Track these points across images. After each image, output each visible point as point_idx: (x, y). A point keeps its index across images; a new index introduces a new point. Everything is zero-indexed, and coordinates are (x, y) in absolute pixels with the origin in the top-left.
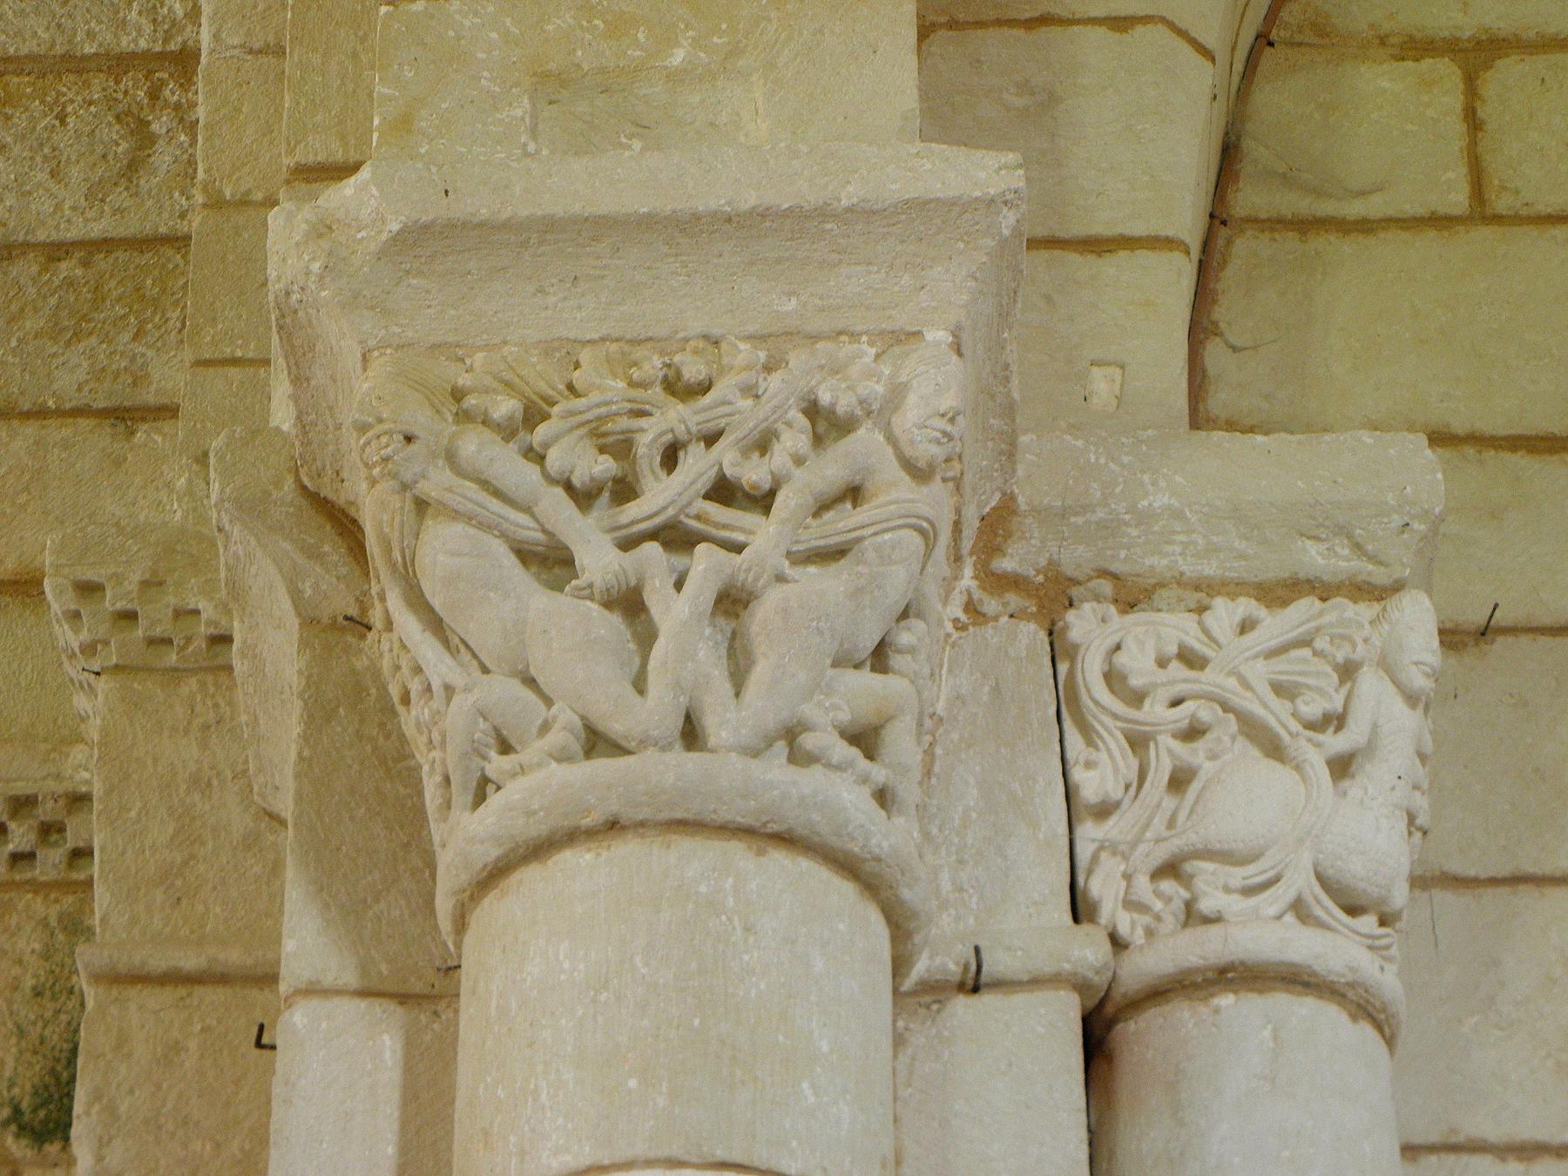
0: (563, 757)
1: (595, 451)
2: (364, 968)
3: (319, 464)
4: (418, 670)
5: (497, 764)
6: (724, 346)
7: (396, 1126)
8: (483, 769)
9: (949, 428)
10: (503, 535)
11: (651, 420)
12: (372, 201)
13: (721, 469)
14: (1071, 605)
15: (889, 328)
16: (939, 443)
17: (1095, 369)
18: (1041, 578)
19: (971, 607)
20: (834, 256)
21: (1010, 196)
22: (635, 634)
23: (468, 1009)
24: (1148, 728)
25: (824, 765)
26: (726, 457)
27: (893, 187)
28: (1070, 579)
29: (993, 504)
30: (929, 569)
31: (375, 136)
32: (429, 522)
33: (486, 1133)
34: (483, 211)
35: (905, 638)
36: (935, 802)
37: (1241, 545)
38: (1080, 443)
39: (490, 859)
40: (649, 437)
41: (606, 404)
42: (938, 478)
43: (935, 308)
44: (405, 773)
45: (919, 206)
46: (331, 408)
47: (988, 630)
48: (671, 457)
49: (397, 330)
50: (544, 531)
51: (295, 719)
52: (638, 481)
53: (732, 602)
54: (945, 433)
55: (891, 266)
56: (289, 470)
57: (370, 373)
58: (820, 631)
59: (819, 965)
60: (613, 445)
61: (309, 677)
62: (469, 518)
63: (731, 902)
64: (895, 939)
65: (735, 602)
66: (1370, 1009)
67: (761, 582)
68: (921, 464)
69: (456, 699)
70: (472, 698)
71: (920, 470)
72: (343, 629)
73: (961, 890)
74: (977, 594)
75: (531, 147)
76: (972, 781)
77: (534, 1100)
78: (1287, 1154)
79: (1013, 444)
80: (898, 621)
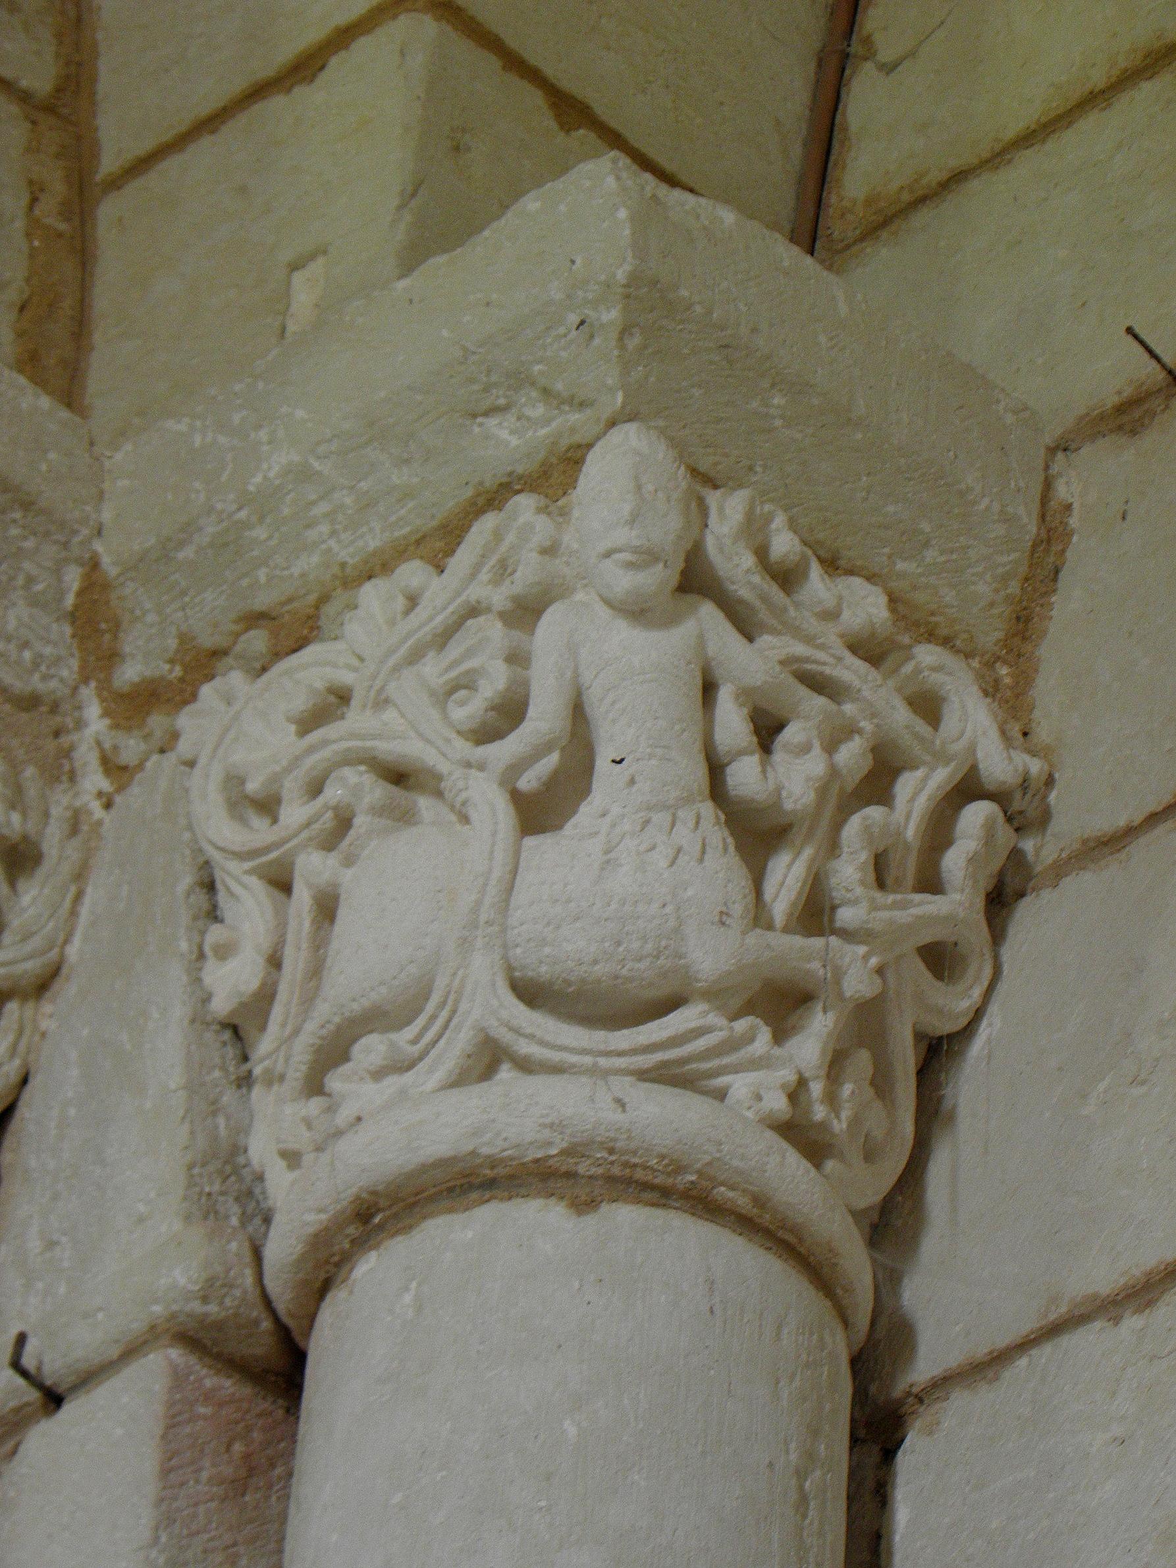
18: (178, 671)
24: (273, 855)
29: (76, 586)
37: (400, 477)
66: (639, 1174)
78: (397, 1498)
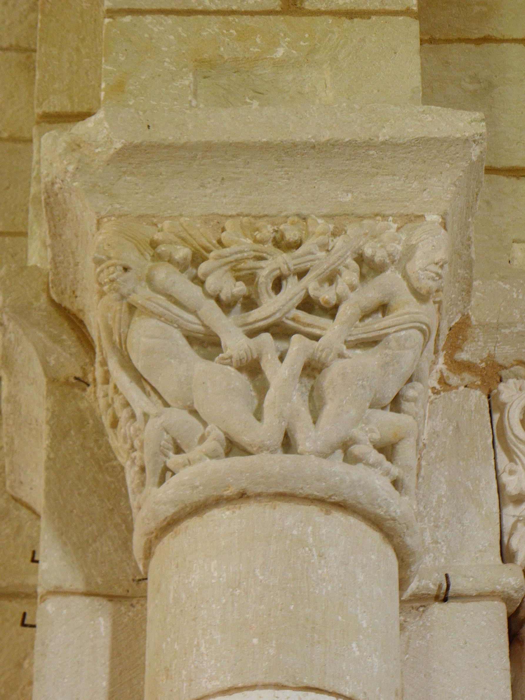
0: (214, 456)
1: (233, 280)
2: (88, 580)
3: (63, 286)
4: (127, 404)
5: (173, 460)
6: (310, 221)
7: (108, 670)
8: (165, 463)
9: (440, 271)
10: (179, 327)
11: (268, 262)
12: (105, 131)
13: (307, 292)
14: (501, 381)
15: (405, 213)
16: (433, 279)
17: (515, 245)
18: (483, 365)
19: (442, 381)
20: (375, 170)
21: (477, 137)
22: (255, 386)
23: (151, 604)
25: (365, 464)
26: (311, 285)
27: (410, 130)
28: (501, 366)
29: (457, 320)
30: (425, 353)
31: (103, 94)
32: (136, 318)
33: (167, 670)
34: (170, 138)
35: (411, 393)
36: (421, 492)
38: (507, 287)
39: (169, 514)
40: (266, 273)
41: (241, 252)
42: (431, 301)
43: (432, 202)
44: (110, 469)
45: (425, 142)
46: (73, 253)
47: (452, 394)
48: (278, 285)
49: (118, 206)
50: (204, 325)
51: (44, 436)
52: (258, 297)
53: (312, 369)
54: (438, 274)
55: (407, 177)
56: (43, 290)
57: (103, 231)
58: (363, 387)
59: (361, 578)
60: (244, 276)
61: (53, 413)
62: (160, 316)
63: (311, 540)
64: (401, 568)
65: (314, 369)
67: (330, 358)
68: (423, 292)
69: (150, 421)
70: (160, 421)
71: (422, 295)
72: (73, 385)
73: (437, 542)
74: (446, 373)
75: (194, 103)
76: (443, 480)
77: (197, 651)
79: (470, 285)
80: (406, 384)
